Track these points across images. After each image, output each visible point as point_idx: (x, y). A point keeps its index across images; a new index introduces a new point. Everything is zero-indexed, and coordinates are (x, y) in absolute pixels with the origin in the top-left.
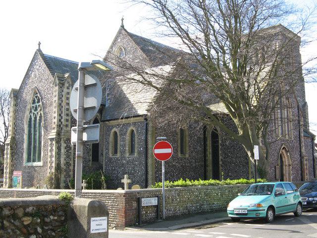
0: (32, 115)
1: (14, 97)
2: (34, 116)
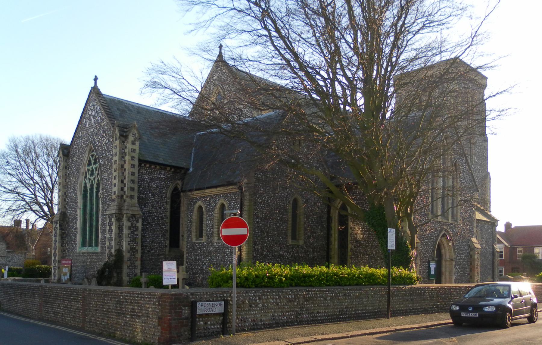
0: (87, 182)
2: (90, 183)
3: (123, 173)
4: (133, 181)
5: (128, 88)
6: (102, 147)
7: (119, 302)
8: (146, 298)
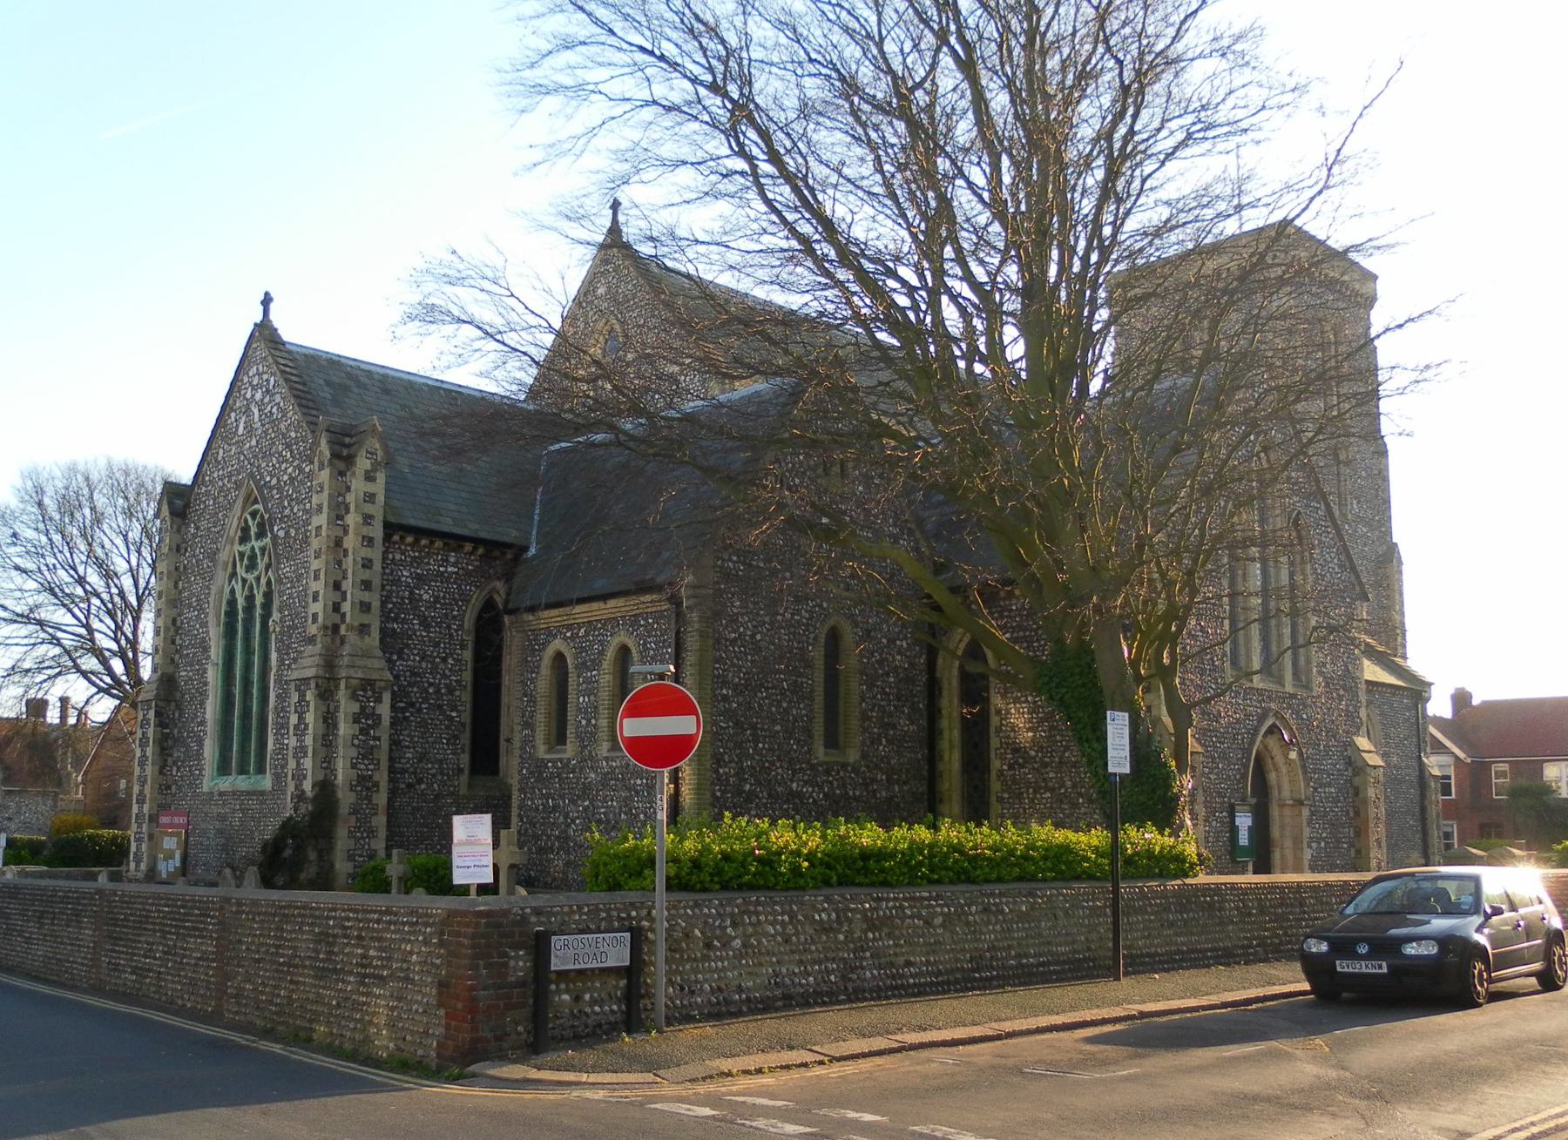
0: (238, 587)
1: (171, 513)
3: (339, 563)
4: (366, 585)
5: (360, 323)
7: (325, 938)
8: (404, 924)
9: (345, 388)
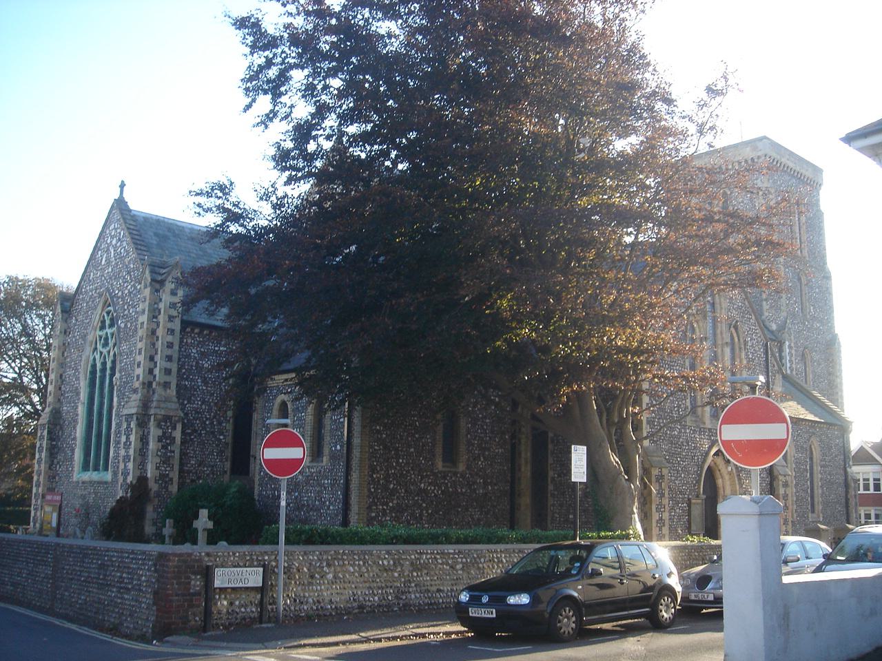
0: (98, 357)
1: (62, 311)
2: (102, 360)
3: (154, 345)
4: (169, 358)
5: (173, 202)
6: (123, 299)
7: (102, 566)
8: (139, 559)
9: (165, 238)
